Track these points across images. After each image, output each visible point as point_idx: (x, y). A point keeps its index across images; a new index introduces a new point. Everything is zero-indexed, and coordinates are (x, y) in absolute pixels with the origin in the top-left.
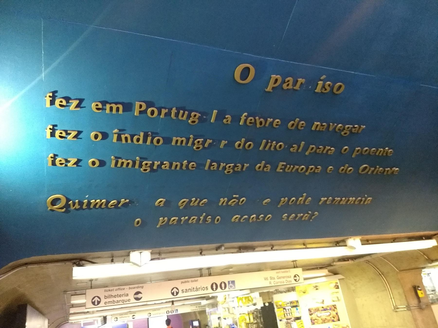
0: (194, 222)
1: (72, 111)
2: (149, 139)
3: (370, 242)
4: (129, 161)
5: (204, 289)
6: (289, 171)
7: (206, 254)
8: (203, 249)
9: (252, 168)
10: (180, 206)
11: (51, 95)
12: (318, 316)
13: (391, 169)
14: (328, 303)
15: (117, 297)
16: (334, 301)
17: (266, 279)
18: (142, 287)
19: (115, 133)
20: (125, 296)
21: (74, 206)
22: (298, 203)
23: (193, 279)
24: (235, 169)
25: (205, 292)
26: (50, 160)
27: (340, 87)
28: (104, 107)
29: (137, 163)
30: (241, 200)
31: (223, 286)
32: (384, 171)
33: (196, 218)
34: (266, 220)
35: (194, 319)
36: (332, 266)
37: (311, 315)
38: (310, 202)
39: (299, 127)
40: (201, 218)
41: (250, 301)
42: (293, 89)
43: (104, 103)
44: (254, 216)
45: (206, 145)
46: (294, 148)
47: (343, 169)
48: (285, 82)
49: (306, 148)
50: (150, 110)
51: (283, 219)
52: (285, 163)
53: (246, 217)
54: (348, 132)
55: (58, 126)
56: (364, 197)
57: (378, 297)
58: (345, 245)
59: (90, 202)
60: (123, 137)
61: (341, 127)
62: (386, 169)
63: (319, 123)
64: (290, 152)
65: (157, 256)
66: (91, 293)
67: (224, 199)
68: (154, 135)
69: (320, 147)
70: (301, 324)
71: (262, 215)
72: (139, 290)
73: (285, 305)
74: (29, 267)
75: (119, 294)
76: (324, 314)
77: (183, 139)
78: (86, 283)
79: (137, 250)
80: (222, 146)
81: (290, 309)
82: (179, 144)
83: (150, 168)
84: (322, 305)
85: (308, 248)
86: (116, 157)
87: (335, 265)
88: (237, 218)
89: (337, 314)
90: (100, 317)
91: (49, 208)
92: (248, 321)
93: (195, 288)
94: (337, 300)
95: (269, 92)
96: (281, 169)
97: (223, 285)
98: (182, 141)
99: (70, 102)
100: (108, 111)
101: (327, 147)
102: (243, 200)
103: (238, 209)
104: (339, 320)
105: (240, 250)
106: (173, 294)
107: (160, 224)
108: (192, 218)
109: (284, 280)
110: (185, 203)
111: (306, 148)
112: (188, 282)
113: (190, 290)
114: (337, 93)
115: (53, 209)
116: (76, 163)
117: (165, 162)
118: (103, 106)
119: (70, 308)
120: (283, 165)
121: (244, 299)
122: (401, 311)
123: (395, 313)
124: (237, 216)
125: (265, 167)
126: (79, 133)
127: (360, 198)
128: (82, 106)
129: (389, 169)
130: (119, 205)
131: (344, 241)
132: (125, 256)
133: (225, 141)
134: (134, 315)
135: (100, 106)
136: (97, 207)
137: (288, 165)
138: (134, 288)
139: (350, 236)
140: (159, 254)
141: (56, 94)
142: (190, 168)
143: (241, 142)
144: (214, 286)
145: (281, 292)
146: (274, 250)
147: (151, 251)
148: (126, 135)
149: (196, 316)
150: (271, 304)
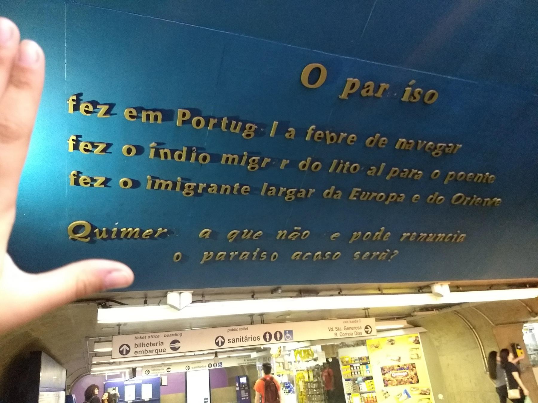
2: (194, 155)
3: (461, 289)
4: (169, 182)
5: (255, 339)
6: (365, 199)
7: (259, 298)
9: (319, 194)
11: (75, 98)
13: (491, 199)
14: (406, 361)
16: (412, 359)
17: (331, 329)
18: (181, 335)
19: (152, 148)
20: (159, 345)
21: (100, 235)
22: (374, 239)
23: (242, 327)
25: (257, 343)
26: (73, 178)
29: (179, 185)
30: (304, 233)
31: (278, 336)
32: (483, 201)
33: (249, 253)
34: (333, 258)
35: (242, 374)
39: (380, 145)
40: (254, 253)
42: (374, 96)
43: (139, 110)
44: (320, 253)
45: (263, 165)
47: (432, 198)
48: (364, 88)
49: (387, 172)
51: (355, 257)
52: (360, 190)
53: (309, 254)
54: (440, 153)
56: (457, 233)
60: (162, 152)
61: (432, 145)
63: (404, 140)
64: (367, 175)
65: (200, 298)
66: (119, 340)
67: (282, 231)
68: (199, 151)
70: (372, 385)
71: (329, 253)
73: (353, 362)
75: (152, 343)
76: (400, 375)
78: (113, 329)
80: (282, 167)
81: (359, 367)
82: (230, 162)
84: (398, 363)
85: (384, 294)
86: (152, 177)
87: (415, 316)
88: (298, 255)
89: (416, 374)
90: (128, 368)
91: (71, 237)
93: (244, 337)
94: (417, 357)
96: (355, 196)
98: (234, 159)
100: (144, 120)
101: (413, 170)
102: (307, 234)
103: (299, 245)
104: (418, 382)
106: (217, 344)
107: (204, 259)
108: (243, 253)
109: (353, 331)
110: (235, 236)
111: (387, 172)
112: (236, 330)
113: (238, 340)
117: (212, 185)
120: (357, 192)
121: (302, 352)
125: (335, 193)
126: (109, 145)
129: (489, 199)
130: (156, 236)
131: (428, 287)
132: (161, 297)
133: (287, 160)
135: (135, 113)
136: (129, 236)
142: (243, 192)
145: (348, 346)
146: (342, 295)
148: (166, 150)
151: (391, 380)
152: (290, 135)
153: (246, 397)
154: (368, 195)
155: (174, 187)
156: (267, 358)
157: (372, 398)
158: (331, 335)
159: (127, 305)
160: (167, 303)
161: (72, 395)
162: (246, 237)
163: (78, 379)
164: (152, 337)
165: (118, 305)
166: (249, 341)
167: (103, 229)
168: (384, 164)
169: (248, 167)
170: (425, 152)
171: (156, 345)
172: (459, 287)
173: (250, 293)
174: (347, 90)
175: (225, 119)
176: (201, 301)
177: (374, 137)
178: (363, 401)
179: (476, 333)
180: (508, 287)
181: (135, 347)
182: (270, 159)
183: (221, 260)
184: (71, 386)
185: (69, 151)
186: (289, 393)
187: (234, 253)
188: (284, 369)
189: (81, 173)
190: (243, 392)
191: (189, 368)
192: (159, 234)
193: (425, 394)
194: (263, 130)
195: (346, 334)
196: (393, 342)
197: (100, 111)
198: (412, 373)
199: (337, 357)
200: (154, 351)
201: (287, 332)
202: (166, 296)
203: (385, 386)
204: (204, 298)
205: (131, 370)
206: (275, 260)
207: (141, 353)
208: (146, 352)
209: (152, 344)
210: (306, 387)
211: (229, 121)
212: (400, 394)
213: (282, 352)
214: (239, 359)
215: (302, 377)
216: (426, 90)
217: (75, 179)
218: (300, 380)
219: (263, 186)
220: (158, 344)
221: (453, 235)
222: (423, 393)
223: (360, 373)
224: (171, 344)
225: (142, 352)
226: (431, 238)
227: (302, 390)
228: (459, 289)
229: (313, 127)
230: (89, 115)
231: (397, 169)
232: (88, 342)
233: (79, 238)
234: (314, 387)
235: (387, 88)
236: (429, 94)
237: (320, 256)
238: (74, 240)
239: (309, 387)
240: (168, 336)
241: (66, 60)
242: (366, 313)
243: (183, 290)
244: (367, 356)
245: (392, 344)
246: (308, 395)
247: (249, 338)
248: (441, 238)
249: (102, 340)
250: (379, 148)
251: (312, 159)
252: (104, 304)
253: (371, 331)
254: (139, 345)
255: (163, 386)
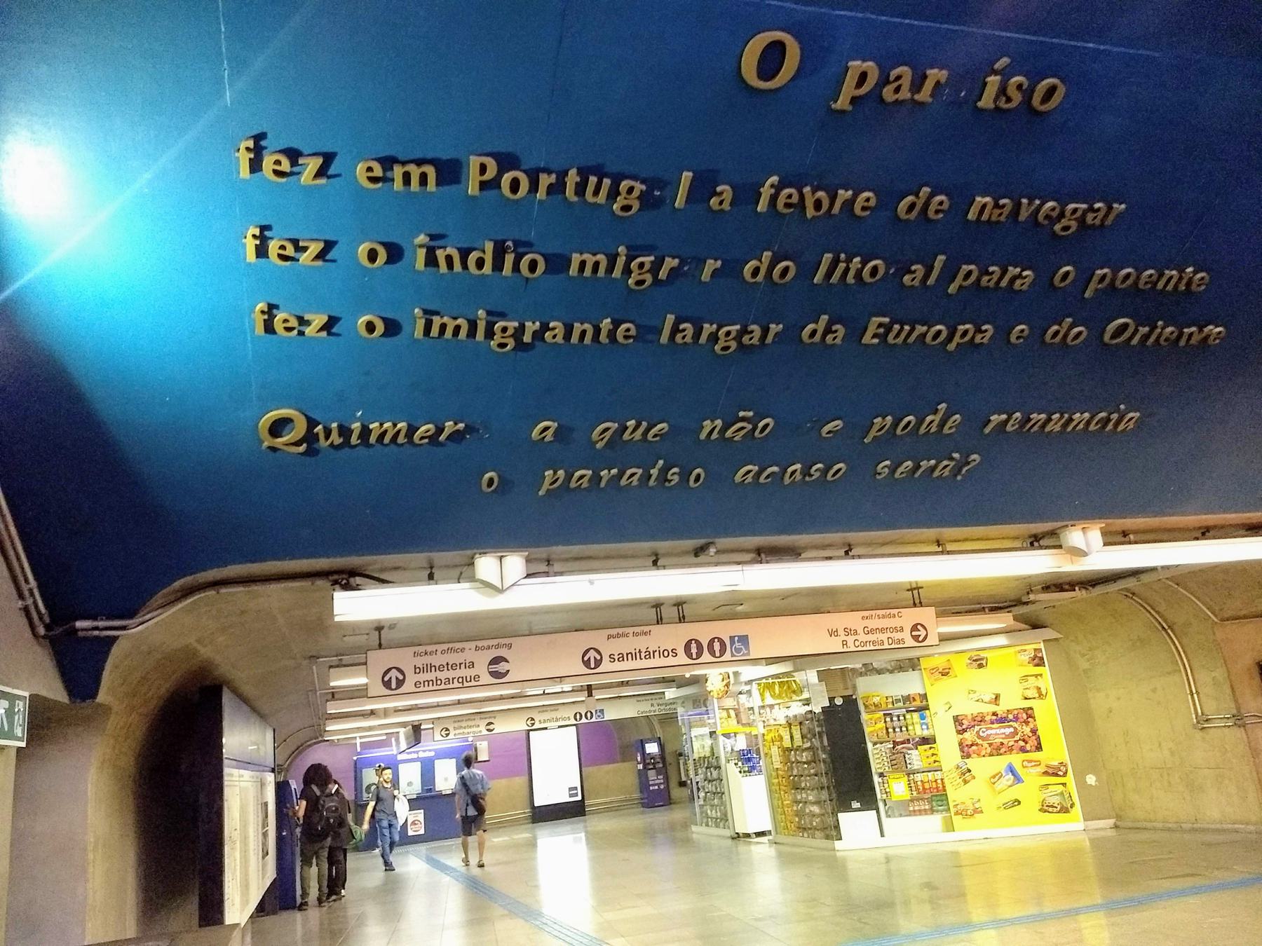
0: (635, 483)
1: (307, 188)
2: (509, 259)
3: (1132, 537)
4: (459, 321)
5: (666, 653)
6: (900, 340)
7: (668, 565)
8: (660, 552)
9: (791, 335)
10: (597, 442)
11: (251, 144)
12: (979, 737)
13: (1201, 330)
14: (1012, 701)
15: (446, 668)
16: (1026, 699)
17: (833, 633)
18: (510, 646)
19: (421, 246)
20: (465, 667)
21: (327, 437)
22: (922, 430)
23: (637, 629)
24: (743, 339)
25: (671, 661)
26: (260, 320)
27: (1052, 90)
28: (389, 174)
29: (481, 326)
30: (761, 425)
31: (717, 647)
32: (1181, 334)
33: (640, 471)
34: (829, 477)
35: (649, 736)
36: (1026, 603)
37: (959, 732)
38: (956, 426)
39: (931, 214)
40: (652, 471)
41: (794, 692)
42: (912, 100)
43: (388, 162)
44: (798, 466)
45: (663, 275)
46: (914, 276)
47: (1057, 333)
48: (887, 82)
49: (949, 273)
50: (507, 179)
51: (879, 474)
52: (887, 320)
53: (775, 469)
54: (1074, 225)
55: (275, 228)
56: (1118, 411)
57: (1154, 690)
58: (1058, 544)
59: (368, 428)
60: (441, 254)
61: (1053, 209)
62: (1185, 330)
63: (988, 199)
64: (902, 285)
65: (543, 568)
66: (381, 660)
67: (712, 421)
68: (521, 250)
69: (991, 269)
70: (933, 755)
71: (820, 466)
72: (502, 652)
73: (890, 706)
74: (224, 591)
75: (450, 663)
76: (998, 733)
77: (600, 257)
78: (366, 637)
79: (491, 552)
80: (706, 276)
81: (904, 716)
82: (588, 272)
83: (515, 340)
84: (993, 708)
85: (949, 553)
86: (426, 312)
87: (1033, 602)
88: (749, 472)
89: (1034, 731)
90: (404, 725)
91: (266, 444)
92: (787, 743)
93: (643, 650)
94: (1037, 695)
95: (843, 112)
96: (875, 336)
97: (717, 646)
98: (596, 265)
99: (300, 162)
100: (398, 185)
101: (1010, 268)
102: (767, 425)
103: (752, 449)
104: (1039, 748)
105: (759, 555)
106: (587, 664)
107: (546, 486)
108: (629, 472)
109: (883, 637)
110: (608, 435)
111: (949, 273)
112: (627, 635)
113: (630, 655)
114: (1043, 108)
115: (276, 446)
116: (328, 326)
117: (551, 325)
118: (385, 170)
119: (327, 701)
120: (880, 325)
121: (777, 687)
122: (1215, 727)
123: (1199, 734)
124: (750, 467)
125: (828, 330)
126: (329, 245)
127: (1103, 415)
128: (331, 171)
129: (1193, 329)
130: (442, 438)
131: (1053, 533)
132: (461, 565)
133: (716, 260)
134: (492, 723)
135: (378, 171)
136: (387, 440)
137: (897, 324)
138: (486, 718)
139: (1072, 519)
140: (547, 564)
141: (263, 143)
142: (620, 338)
143: (760, 261)
144: (693, 649)
145: (879, 672)
146: (853, 557)
147: (527, 553)
148: (449, 251)
149: (652, 729)
150: (850, 702)
151: (977, 745)
152: (721, 203)
153: (658, 785)
154: (907, 332)
155: (472, 332)
156: (702, 702)
157: (934, 783)
158: (834, 645)
159: (393, 582)
160: (474, 577)
161: (290, 781)
162: (632, 436)
163: (300, 750)
164: (449, 651)
165: (375, 584)
166: (654, 658)
167: (331, 425)
168: (941, 258)
169: (630, 281)
170: (1036, 223)
171: (458, 667)
172: (1128, 534)
173: (650, 556)
174: (849, 89)
175: (573, 173)
176: (544, 574)
177: (917, 195)
178: (914, 789)
179: (1174, 639)
180: (1246, 533)
181: (415, 673)
182: (677, 261)
183: (583, 486)
184: (286, 766)
185: (248, 260)
186: (751, 774)
187: (609, 471)
188: (738, 723)
189: (276, 307)
190: (652, 774)
191: (533, 722)
192: (446, 436)
193: (1056, 775)
194: (659, 193)
195: (868, 643)
196: (984, 662)
197: (305, 170)
198: (1027, 730)
199: (854, 694)
200: (455, 680)
201: (736, 638)
202: (473, 564)
203: (963, 757)
204: (551, 567)
205: (409, 730)
206: (697, 485)
207: (428, 686)
208: (439, 682)
209: (450, 666)
210: (786, 760)
211: (581, 177)
212: (997, 775)
213: (731, 687)
214: (638, 703)
215: (778, 739)
216: (1035, 79)
217: (265, 320)
218: (773, 745)
219: (665, 322)
220: (463, 666)
221: (1110, 414)
222: (1050, 771)
223: (907, 730)
224: (490, 664)
225: (431, 683)
226: (1056, 424)
227: (777, 765)
228: (1127, 539)
229: (774, 179)
230: (284, 180)
231: (972, 267)
232: (316, 667)
233: (287, 445)
234: (804, 760)
235: (943, 81)
236: (1043, 86)
237: (798, 473)
238: (273, 449)
239: (793, 760)
240: (483, 648)
241: (225, 62)
242: (915, 596)
243: (508, 552)
244: (922, 692)
245: (981, 666)
246: (790, 776)
247: (654, 652)
248: (1079, 423)
249: (344, 663)
250: (929, 220)
251: (773, 255)
252: (344, 581)
253: (927, 635)
254: (423, 668)
255: (480, 762)
